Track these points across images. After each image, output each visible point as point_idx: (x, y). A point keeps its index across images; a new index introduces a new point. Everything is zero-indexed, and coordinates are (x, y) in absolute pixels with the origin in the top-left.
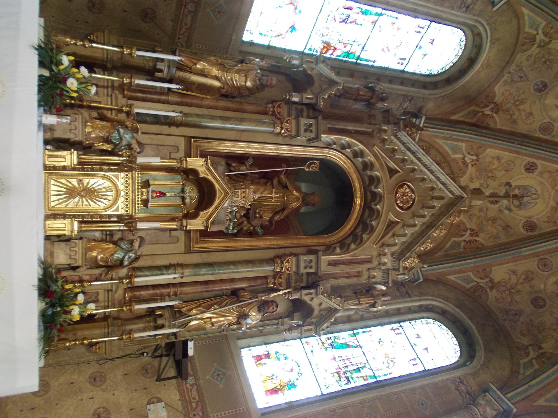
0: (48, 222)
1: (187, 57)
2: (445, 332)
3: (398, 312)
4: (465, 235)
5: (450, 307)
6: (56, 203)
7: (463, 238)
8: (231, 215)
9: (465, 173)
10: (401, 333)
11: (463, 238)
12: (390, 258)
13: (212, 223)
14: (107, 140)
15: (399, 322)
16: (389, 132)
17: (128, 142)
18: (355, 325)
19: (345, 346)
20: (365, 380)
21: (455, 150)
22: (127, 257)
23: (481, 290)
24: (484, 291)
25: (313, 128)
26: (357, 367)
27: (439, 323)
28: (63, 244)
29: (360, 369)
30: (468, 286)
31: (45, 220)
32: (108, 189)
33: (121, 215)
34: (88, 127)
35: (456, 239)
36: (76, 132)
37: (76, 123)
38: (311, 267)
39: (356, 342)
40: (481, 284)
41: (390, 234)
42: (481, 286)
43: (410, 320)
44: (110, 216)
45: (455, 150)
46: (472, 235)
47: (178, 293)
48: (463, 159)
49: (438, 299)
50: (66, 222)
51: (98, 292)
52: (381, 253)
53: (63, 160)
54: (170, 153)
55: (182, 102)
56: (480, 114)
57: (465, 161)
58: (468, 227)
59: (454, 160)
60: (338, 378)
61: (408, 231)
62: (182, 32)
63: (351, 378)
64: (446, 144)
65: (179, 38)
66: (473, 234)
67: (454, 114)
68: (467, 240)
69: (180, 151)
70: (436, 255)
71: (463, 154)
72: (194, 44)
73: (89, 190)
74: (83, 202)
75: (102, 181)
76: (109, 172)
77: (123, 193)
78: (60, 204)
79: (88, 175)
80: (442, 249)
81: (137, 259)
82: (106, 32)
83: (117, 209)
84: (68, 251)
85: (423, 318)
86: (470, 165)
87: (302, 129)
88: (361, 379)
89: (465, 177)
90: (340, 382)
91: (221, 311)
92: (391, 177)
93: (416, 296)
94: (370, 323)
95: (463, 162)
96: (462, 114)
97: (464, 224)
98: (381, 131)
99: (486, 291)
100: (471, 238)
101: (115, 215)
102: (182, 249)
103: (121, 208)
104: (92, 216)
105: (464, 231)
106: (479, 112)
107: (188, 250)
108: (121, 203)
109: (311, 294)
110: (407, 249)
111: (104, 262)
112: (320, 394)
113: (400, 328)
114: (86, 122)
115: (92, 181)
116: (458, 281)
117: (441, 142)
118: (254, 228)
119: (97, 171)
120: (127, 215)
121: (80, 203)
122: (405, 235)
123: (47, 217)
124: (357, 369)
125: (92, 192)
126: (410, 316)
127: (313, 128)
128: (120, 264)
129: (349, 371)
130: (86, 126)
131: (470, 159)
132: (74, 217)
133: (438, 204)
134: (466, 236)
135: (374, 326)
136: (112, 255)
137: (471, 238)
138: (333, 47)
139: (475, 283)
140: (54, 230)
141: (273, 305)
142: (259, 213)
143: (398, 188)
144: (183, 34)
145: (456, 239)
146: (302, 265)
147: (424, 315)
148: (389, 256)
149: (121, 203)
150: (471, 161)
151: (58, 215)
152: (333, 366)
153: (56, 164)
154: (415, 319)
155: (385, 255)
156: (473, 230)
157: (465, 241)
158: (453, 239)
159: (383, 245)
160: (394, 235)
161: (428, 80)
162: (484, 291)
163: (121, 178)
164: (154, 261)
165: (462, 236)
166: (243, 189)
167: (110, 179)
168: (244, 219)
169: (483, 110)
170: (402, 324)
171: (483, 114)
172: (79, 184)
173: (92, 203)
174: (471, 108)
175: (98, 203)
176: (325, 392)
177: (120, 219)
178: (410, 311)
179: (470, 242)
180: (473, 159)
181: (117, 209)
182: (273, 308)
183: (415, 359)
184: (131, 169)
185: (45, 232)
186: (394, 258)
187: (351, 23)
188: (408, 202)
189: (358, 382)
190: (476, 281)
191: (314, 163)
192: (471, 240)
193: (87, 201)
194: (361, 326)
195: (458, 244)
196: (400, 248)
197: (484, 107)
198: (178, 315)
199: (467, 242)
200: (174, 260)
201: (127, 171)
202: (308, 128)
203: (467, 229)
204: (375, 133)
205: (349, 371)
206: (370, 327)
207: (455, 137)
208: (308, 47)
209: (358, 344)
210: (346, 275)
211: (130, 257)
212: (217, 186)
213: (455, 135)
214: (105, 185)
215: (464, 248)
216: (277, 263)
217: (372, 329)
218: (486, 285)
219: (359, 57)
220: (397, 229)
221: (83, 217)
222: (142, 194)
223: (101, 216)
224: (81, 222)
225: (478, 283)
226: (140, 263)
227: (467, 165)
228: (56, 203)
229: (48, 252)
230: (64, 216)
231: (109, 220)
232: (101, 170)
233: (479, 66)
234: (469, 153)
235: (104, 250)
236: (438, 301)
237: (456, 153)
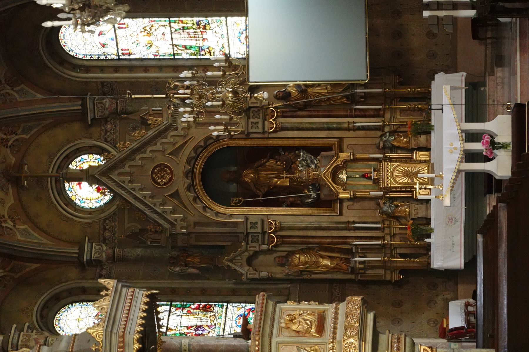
0: (428, 159)
1: (342, 269)
2: (69, 45)
3: (117, 69)
4: (14, 141)
5: (57, 69)
6: (425, 169)
7: (17, 137)
8: (303, 163)
9: (10, 209)
10: (122, 50)
11: (17, 137)
12: (179, 126)
13: (333, 156)
14: (397, 206)
15: (119, 59)
16: (178, 227)
17: (385, 206)
18: (172, 63)
19: (188, 47)
20: (182, 21)
21: (24, 232)
22: (387, 137)
23: (10, 82)
24: (7, 80)
25: (249, 226)
26: (184, 31)
27: (71, 53)
28: (421, 146)
29: (182, 29)
30: (22, 86)
31: (430, 160)
32: (397, 177)
33: (390, 162)
34: (408, 211)
35: (24, 136)
36: (414, 208)
37: (414, 213)
38: (252, 122)
39: (175, 49)
40: (9, 88)
41: (177, 146)
42: (10, 86)
43: (106, 60)
44: (396, 161)
45: (24, 232)
46: (7, 140)
47: (349, 111)
48: (15, 223)
49: (69, 77)
50: (420, 159)
51: (400, 116)
52: (186, 130)
53: (421, 193)
54: (353, 205)
55: (346, 239)
56: (7, 269)
57: (12, 222)
58: (8, 150)
59: (24, 223)
60: (207, 25)
61: (159, 147)
62: (337, 298)
63: (194, 24)
64: (38, 239)
65: (338, 294)
66: (5, 142)
67: (36, 269)
68: (14, 135)
69: (347, 206)
70: (52, 121)
71: (16, 229)
72: (327, 292)
73: (408, 176)
74: (411, 169)
75: (401, 181)
76: (397, 187)
77: (390, 174)
78: (423, 168)
79: (408, 184)
80: (43, 127)
81: (381, 136)
82: (394, 281)
83: (393, 165)
84: (419, 142)
85: (87, 60)
86: (6, 217)
87: (259, 225)
88: (185, 22)
89: (9, 204)
90: (206, 22)
91: (320, 97)
92: (177, 190)
93: (93, 82)
94: (154, 63)
95: (14, 221)
96: (28, 269)
97: (12, 153)
98: (186, 228)
99: (5, 80)
100: (9, 137)
101: (394, 162)
102: (345, 140)
103: (391, 166)
104: (406, 162)
105: (13, 145)
106: (9, 271)
107: (341, 139)
108: (391, 169)
109: (251, 103)
110: (162, 133)
111: (398, 135)
112: (229, 18)
113: (120, 54)
114: (409, 214)
115: (406, 181)
116: (33, 92)
117: (45, 241)
118: (285, 154)
119: (403, 187)
120: (387, 162)
121: (412, 169)
122: (162, 143)
123: (429, 161)
124: (185, 29)
125: (406, 175)
126: (104, 63)
127: (249, 226)
128: (392, 133)
129: (194, 29)
130: (409, 212)
131: (8, 223)
132: (415, 161)
133: (127, 169)
134: (13, 139)
135: (149, 59)
136: (395, 139)
137: (9, 137)
138: (201, 310)
139: (15, 89)
140: (426, 155)
141: (279, 97)
142: (284, 165)
143: (160, 185)
144: (336, 297)
145: (24, 136)
146: (260, 125)
147: (85, 63)
148: (180, 128)
149: (391, 169)
150: (6, 221)
151: (424, 163)
152: (208, 34)
153: (424, 191)
154: (98, 60)
155: (183, 129)
156: (4, 146)
157: (16, 135)
158: (27, 137)
159: (184, 136)
160: (174, 144)
161: (83, 297)
162: (7, 80)
163: (391, 183)
164: (365, 133)
165: (17, 140)
166: (310, 179)
167: (397, 183)
168: (294, 161)
169: (5, 273)
170: (116, 57)
171: (4, 269)
172: (413, 179)
173: (406, 169)
174: (19, 274)
175: (402, 169)
176: (223, 19)
177: (390, 160)
178: (102, 69)
179: (12, 133)
180: (5, 223)
181: (393, 165)
182: (279, 94)
183: (119, 28)
184: (385, 188)
185: (430, 154)
186: (176, 126)
187: (192, 327)
188: (158, 171)
189: (188, 21)
190: (14, 91)
191: (235, 203)
192: (9, 135)
193: (409, 170)
194: (163, 61)
195: (24, 132)
196: (168, 133)
197: (5, 276)
198: (350, 97)
199: (14, 133)
200: (352, 134)
201: (387, 187)
202: (253, 225)
203: (10, 147)
204: (192, 226)
205: (194, 29)
206: (154, 59)
207: (36, 245)
208: (225, 307)
209: (174, 47)
210: (212, 113)
211: (385, 137)
212: (330, 180)
213: (37, 247)
214: (399, 179)
215: (19, 127)
216: (279, 127)
217: (153, 57)
218: (4, 86)
219: (171, 307)
220: (170, 149)
221: (411, 161)
222: (377, 175)
223: (401, 161)
224: (412, 158)
225: (12, 89)
226: (379, 133)
227: (9, 217)
228: (425, 169)
229: (429, 141)
230: (421, 162)
231: (397, 160)
232: (401, 188)
233: (35, 310)
234: (11, 229)
235: (400, 141)
236: (69, 75)
237: (24, 230)
